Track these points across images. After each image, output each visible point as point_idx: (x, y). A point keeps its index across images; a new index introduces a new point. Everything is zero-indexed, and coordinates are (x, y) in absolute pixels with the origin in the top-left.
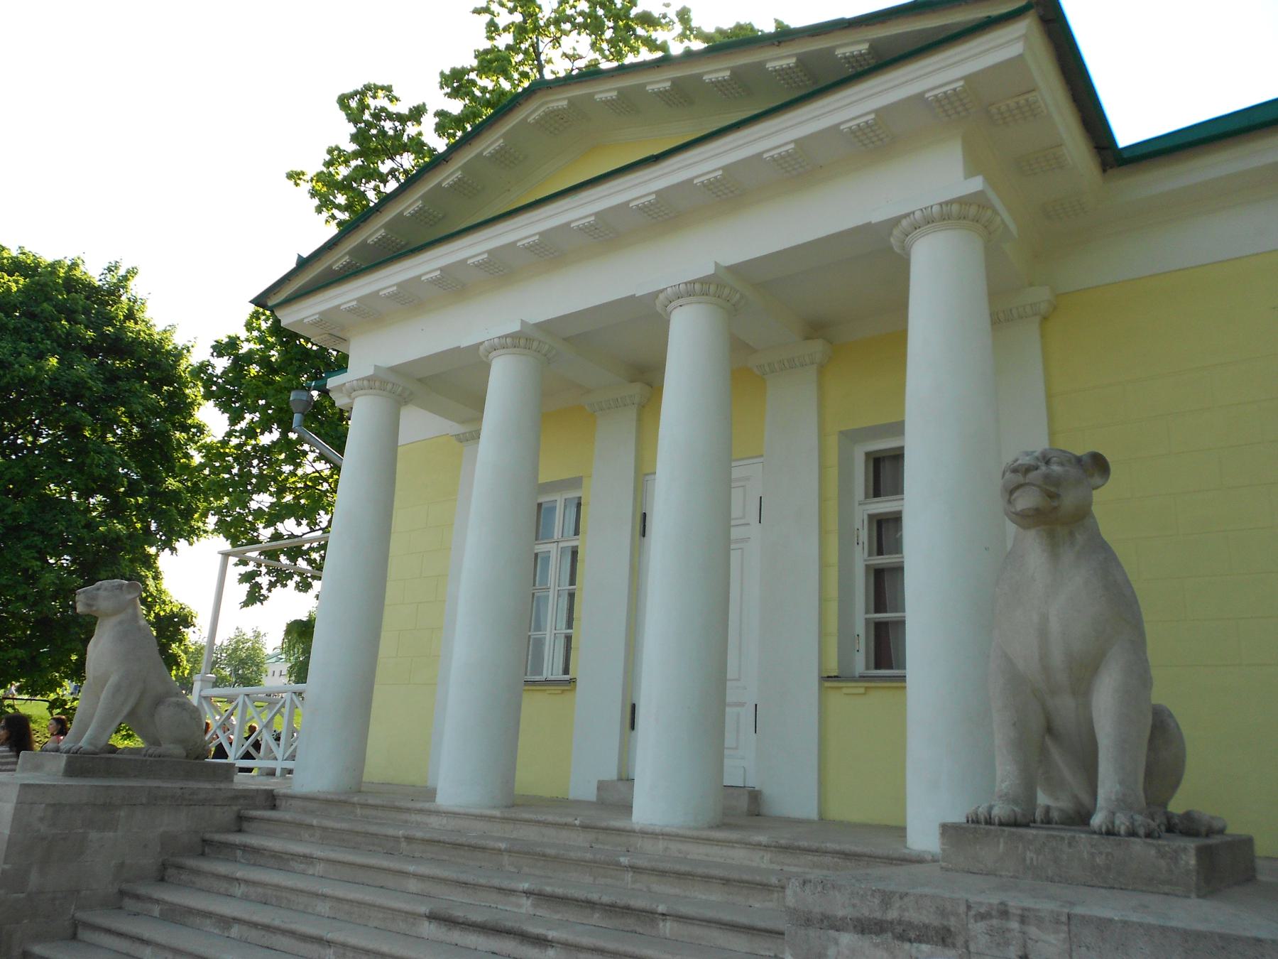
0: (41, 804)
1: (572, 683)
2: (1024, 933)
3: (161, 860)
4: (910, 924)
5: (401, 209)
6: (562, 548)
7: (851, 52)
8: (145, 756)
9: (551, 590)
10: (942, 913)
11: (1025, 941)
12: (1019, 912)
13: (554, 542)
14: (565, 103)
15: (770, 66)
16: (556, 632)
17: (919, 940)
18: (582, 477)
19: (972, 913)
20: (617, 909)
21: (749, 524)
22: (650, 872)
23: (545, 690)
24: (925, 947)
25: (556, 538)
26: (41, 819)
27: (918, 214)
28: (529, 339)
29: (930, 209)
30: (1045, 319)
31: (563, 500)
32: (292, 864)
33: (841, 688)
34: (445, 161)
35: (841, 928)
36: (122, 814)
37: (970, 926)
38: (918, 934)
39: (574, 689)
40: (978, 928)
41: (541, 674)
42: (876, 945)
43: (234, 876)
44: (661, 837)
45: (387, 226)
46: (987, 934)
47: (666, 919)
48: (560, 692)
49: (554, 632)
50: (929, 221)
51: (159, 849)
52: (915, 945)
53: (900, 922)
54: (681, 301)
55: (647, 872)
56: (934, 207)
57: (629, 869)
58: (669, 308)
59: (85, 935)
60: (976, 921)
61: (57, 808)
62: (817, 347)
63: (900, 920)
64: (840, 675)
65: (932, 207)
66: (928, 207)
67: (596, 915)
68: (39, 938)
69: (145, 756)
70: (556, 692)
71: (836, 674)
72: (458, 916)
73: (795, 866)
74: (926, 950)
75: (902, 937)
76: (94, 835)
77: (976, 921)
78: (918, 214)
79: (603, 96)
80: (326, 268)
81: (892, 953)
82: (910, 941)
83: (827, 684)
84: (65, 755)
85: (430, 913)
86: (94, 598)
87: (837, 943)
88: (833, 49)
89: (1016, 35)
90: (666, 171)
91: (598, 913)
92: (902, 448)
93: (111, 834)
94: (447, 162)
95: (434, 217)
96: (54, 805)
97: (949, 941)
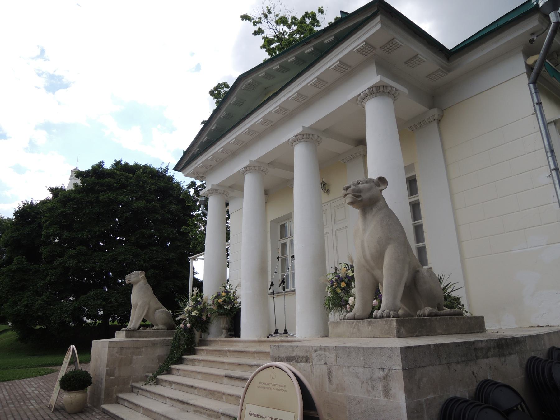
0: (116, 347)
2: (325, 355)
3: (159, 365)
5: (210, 129)
7: (329, 41)
8: (152, 330)
10: (306, 351)
11: (326, 358)
12: (324, 348)
13: (288, 238)
14: (251, 80)
15: (326, 42)
23: (288, 294)
24: (302, 364)
26: (117, 353)
27: (362, 94)
28: (255, 167)
30: (439, 121)
31: (289, 222)
32: (196, 363)
34: (219, 109)
36: (143, 349)
37: (313, 355)
40: (314, 355)
43: (176, 368)
45: (207, 135)
46: (317, 357)
48: (292, 294)
51: (157, 361)
52: (300, 363)
53: (297, 356)
54: (296, 143)
58: (293, 145)
59: (136, 390)
61: (121, 349)
65: (365, 90)
68: (121, 391)
69: (152, 330)
70: (292, 294)
72: (232, 375)
73: (276, 341)
75: (297, 362)
76: (135, 357)
77: (314, 353)
78: (362, 94)
79: (275, 68)
80: (193, 153)
82: (299, 362)
84: (125, 331)
85: (225, 375)
86: (130, 278)
88: (323, 41)
89: (378, 21)
90: (280, 97)
92: (415, 176)
93: (141, 356)
94: (220, 109)
95: (218, 128)
96: (120, 348)
97: (308, 361)
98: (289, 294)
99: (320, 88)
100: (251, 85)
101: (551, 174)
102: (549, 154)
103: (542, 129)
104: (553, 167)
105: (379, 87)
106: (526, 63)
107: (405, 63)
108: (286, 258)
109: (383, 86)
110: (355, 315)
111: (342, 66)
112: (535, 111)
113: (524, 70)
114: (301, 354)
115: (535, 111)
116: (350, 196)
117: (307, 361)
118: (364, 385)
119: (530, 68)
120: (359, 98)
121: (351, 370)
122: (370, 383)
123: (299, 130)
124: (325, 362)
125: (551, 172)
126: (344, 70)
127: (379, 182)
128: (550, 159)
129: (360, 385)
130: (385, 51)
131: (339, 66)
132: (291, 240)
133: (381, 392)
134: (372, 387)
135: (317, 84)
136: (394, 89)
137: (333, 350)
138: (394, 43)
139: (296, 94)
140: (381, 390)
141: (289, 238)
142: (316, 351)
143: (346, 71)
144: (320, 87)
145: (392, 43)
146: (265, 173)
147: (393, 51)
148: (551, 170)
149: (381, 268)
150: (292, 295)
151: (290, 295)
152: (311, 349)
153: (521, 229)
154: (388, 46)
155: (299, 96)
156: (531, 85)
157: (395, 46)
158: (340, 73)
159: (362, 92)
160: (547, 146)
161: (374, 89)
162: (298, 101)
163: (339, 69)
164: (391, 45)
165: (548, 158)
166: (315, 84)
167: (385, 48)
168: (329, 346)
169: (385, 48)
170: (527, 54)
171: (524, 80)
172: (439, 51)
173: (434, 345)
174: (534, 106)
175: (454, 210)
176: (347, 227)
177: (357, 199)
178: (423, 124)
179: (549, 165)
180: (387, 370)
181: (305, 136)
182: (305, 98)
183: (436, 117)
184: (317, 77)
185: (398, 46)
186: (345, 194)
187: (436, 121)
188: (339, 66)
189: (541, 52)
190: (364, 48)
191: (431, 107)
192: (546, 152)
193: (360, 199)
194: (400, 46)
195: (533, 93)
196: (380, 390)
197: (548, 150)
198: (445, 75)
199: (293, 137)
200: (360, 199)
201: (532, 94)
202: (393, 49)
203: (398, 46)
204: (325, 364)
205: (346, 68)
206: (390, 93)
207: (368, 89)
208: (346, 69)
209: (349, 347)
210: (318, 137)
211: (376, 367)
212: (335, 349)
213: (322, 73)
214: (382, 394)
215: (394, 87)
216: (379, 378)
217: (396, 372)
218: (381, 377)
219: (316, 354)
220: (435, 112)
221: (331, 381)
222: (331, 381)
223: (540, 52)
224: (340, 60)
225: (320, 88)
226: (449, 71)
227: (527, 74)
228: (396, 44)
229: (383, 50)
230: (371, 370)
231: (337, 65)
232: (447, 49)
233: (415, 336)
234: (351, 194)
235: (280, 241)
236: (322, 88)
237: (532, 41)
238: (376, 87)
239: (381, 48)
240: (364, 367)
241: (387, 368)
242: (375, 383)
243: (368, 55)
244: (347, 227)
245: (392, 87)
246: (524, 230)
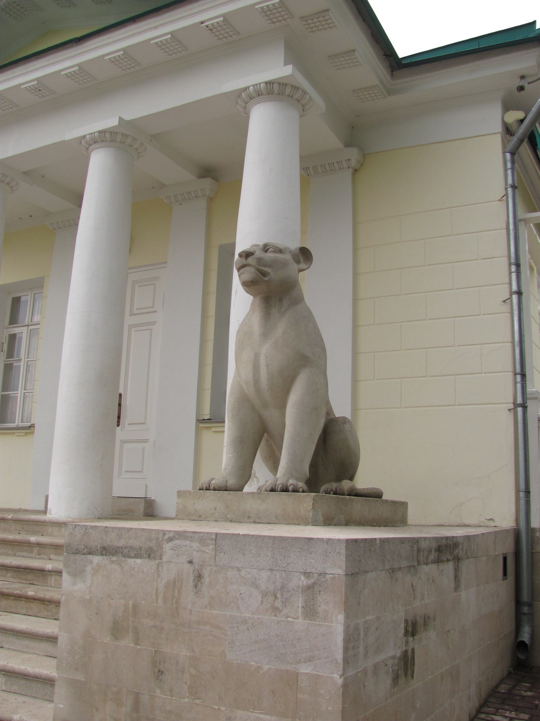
1: (32, 427)
4: (131, 547)
6: (31, 330)
9: (23, 361)
16: (25, 391)
17: (137, 556)
18: (44, 277)
19: (166, 537)
20: (21, 570)
21: (156, 311)
22: (50, 547)
24: (139, 561)
25: (27, 322)
27: (251, 88)
29: (259, 85)
30: (356, 171)
31: (33, 295)
33: (210, 428)
35: (94, 553)
38: (135, 553)
39: (33, 433)
41: (14, 422)
42: (113, 562)
44: (63, 525)
47: (52, 574)
48: (24, 434)
49: (23, 391)
50: (259, 94)
55: (48, 546)
56: (261, 85)
57: (37, 545)
60: (168, 543)
62: (207, 183)
63: (126, 546)
64: (211, 419)
66: (258, 84)
67: (9, 575)
71: (208, 418)
74: (139, 562)
78: (251, 88)
81: (121, 566)
83: (201, 425)
87: (91, 563)
90: (85, 50)
91: (10, 573)
97: (152, 555)
98: (16, 434)
99: (171, 55)
100: (18, 5)
101: (510, 298)
102: (513, 268)
103: (511, 227)
104: (514, 288)
105: (284, 85)
106: (503, 119)
107: (330, 57)
108: (13, 363)
109: (292, 86)
110: (226, 483)
111: (225, 27)
112: (506, 195)
113: (499, 128)
114: (136, 543)
115: (506, 195)
116: (252, 270)
117: (149, 557)
118: (267, 599)
119: (508, 130)
120: (243, 95)
121: (243, 573)
122: (279, 596)
123: (112, 122)
124: (189, 559)
125: (511, 295)
126: (226, 35)
127: (299, 254)
128: (514, 276)
129: (260, 598)
130: (307, 26)
131: (221, 27)
132: (31, 330)
133: (300, 610)
134: (282, 602)
135: (168, 45)
136: (308, 96)
137: (210, 539)
138: (327, 18)
139: (122, 53)
140: (300, 606)
141: (28, 325)
142: (170, 539)
143: (229, 38)
144: (171, 53)
145: (324, 17)
146: (12, 191)
147: (319, 30)
148: (511, 293)
149: (282, 406)
150: (23, 436)
151: (18, 436)
152: (161, 536)
153: (451, 375)
154: (315, 20)
155: (126, 58)
156: (508, 156)
157: (326, 24)
158: (217, 38)
159: (254, 86)
160: (513, 255)
161: (276, 86)
162: (119, 67)
163: (218, 31)
164: (321, 19)
165: (510, 273)
166: (165, 45)
167: (310, 22)
168: (201, 532)
169: (310, 22)
170: (507, 107)
171: (496, 143)
172: (384, 55)
173: (381, 539)
174: (506, 189)
175: (355, 326)
176: (154, 323)
177: (263, 278)
178: (328, 169)
179: (510, 284)
180: (316, 575)
181: (119, 138)
182: (136, 65)
183: (353, 163)
184: (172, 33)
185: (331, 25)
186: (241, 265)
187: (351, 170)
188: (221, 27)
189: (533, 109)
190: (275, 9)
191: (348, 144)
192: (510, 264)
193: (266, 279)
194: (335, 26)
195: (508, 168)
196: (298, 607)
197: (513, 260)
198: (382, 98)
199: (94, 133)
200: (266, 279)
201: (506, 170)
202: (321, 27)
203: (331, 25)
204: (191, 562)
205: (231, 33)
206: (299, 101)
207: (266, 83)
208: (231, 36)
209: (244, 535)
210: (142, 144)
211: (295, 570)
212: (214, 537)
213: (183, 29)
214: (301, 613)
215: (307, 94)
216: (299, 587)
217: (334, 579)
218: (303, 586)
219: (171, 544)
220: (353, 154)
221: (198, 591)
222: (198, 591)
223: (532, 108)
224: (225, 16)
225: (171, 55)
226: (390, 92)
227: (501, 135)
228: (329, 21)
229: (305, 23)
230: (284, 574)
231: (218, 23)
232: (398, 56)
233: (333, 524)
234: (254, 266)
235: (9, 330)
236: (174, 55)
237: (521, 88)
238: (280, 84)
239: (302, 18)
240: (271, 570)
241: (317, 571)
242: (291, 596)
243: (278, 23)
244: (154, 323)
245: (305, 93)
246: (454, 376)
